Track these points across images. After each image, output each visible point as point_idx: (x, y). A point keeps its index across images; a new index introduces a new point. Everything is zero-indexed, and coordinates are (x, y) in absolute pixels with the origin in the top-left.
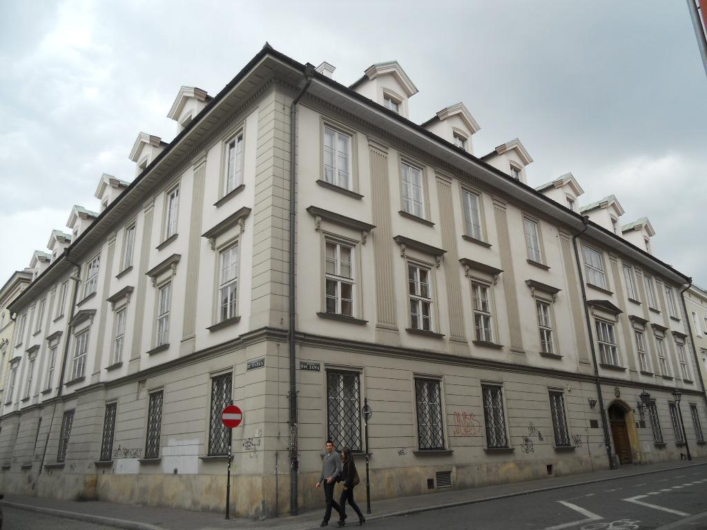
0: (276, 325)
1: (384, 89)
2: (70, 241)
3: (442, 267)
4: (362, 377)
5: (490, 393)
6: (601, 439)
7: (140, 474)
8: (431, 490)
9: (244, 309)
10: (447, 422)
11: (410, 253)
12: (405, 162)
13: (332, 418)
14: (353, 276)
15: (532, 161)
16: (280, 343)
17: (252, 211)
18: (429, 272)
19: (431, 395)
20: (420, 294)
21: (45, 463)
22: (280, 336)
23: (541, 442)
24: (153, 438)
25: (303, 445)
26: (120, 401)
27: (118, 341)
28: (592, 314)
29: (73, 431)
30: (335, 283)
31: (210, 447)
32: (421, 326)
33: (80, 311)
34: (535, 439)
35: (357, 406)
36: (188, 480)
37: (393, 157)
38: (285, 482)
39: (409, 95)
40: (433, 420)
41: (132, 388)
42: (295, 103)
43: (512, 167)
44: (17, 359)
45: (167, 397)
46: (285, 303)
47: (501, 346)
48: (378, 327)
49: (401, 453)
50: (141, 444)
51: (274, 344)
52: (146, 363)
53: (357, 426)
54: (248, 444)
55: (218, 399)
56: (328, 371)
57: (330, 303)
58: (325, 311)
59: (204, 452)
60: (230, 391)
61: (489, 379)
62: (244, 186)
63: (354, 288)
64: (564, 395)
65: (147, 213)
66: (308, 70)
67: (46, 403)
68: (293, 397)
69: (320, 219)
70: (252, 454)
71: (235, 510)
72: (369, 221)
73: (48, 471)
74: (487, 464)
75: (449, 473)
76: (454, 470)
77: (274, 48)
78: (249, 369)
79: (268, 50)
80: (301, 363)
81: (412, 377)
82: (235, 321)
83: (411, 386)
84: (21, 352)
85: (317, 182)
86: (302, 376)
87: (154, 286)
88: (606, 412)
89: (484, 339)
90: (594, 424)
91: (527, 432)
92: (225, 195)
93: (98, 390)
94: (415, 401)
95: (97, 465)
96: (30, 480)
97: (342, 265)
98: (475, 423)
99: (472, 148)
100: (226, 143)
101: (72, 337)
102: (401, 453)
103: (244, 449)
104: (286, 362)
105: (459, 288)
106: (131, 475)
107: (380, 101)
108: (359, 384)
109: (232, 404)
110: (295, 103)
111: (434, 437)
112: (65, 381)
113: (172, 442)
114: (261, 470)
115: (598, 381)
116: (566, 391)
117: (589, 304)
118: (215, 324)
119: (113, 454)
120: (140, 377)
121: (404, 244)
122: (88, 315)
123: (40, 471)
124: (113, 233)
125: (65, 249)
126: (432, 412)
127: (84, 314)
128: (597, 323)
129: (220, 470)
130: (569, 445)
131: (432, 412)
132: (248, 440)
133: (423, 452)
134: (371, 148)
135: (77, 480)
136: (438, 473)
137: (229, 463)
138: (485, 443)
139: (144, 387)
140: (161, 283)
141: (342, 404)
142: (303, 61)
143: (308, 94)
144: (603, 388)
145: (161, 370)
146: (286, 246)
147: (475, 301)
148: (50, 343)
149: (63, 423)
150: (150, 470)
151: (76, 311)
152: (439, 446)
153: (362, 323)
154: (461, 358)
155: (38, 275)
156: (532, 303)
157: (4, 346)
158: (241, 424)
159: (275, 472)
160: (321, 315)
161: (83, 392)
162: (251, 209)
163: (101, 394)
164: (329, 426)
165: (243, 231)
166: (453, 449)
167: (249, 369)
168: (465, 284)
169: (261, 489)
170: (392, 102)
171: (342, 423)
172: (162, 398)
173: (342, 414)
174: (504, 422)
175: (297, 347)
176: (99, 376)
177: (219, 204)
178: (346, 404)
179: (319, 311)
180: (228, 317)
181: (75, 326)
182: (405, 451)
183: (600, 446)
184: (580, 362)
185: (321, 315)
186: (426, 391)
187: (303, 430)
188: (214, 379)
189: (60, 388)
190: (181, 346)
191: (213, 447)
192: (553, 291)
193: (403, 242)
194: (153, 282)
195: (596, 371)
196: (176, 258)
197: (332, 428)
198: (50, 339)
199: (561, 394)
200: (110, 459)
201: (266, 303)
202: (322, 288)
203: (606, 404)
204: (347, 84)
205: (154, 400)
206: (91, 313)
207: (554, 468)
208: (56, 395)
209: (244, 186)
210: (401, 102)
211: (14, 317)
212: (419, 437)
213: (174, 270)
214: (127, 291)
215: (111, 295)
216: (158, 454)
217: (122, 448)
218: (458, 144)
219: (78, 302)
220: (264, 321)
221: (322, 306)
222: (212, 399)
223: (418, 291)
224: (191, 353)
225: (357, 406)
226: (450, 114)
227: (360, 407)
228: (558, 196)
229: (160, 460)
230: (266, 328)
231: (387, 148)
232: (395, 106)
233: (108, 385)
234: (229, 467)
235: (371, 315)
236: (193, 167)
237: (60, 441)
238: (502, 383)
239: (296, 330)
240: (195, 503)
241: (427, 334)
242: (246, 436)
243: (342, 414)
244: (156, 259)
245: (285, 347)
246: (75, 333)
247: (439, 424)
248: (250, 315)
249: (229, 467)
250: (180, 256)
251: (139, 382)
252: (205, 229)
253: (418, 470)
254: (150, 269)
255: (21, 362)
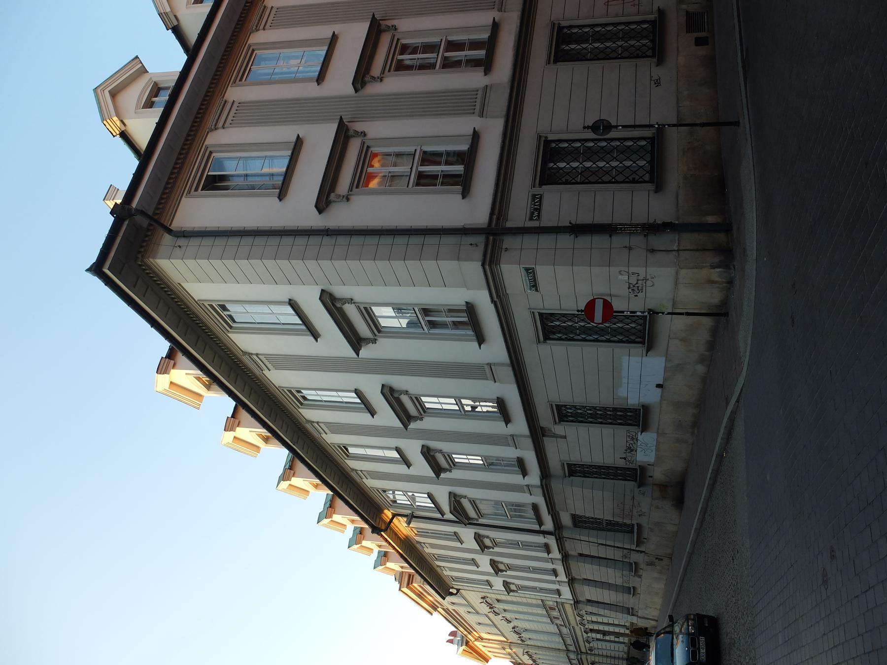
0: (479, 253)
2: (362, 528)
3: (395, 22)
4: (551, 137)
7: (657, 433)
9: (457, 297)
10: (617, 16)
11: (376, 70)
12: (242, 77)
14: (411, 149)
16: (504, 247)
17: (323, 288)
19: (580, 39)
20: (435, 55)
21: (634, 547)
22: (493, 247)
25: (640, 217)
26: (566, 458)
27: (492, 464)
29: (598, 515)
32: (481, 53)
33: (451, 512)
35: (591, 144)
36: (671, 370)
37: (235, 93)
40: (613, 37)
41: (549, 444)
42: (169, 231)
44: (506, 584)
45: (566, 398)
48: (481, 115)
49: (658, 83)
50: (621, 432)
51: (504, 256)
52: (519, 425)
53: (618, 143)
54: (634, 289)
56: (542, 184)
57: (449, 179)
59: (638, 349)
60: (564, 315)
62: (290, 300)
65: (327, 431)
66: (120, 213)
67: (561, 548)
68: (577, 230)
69: (332, 195)
70: (649, 283)
73: (643, 543)
75: (688, 14)
76: (684, 7)
77: (94, 261)
79: (96, 269)
80: (531, 219)
81: (553, 66)
82: (470, 309)
83: (565, 69)
84: (498, 582)
86: (547, 220)
87: (421, 419)
92: (304, 327)
93: (550, 487)
94: (587, 62)
96: (650, 564)
97: (395, 165)
100: (231, 327)
101: (482, 521)
102: (658, 83)
103: (641, 295)
104: (529, 241)
106: (658, 442)
108: (561, 141)
109: (582, 311)
110: (169, 231)
113: (622, 392)
114: (672, 270)
118: (475, 338)
119: (631, 466)
120: (537, 434)
121: (364, 77)
122: (456, 501)
123: (641, 552)
124: (353, 474)
125: (372, 532)
132: (630, 290)
133: (658, 54)
134: (227, 124)
135: (657, 508)
136: (688, 31)
137: (658, 313)
139: (550, 430)
141: (588, 164)
142: (109, 221)
143: (155, 214)
149: (586, 528)
150: (655, 417)
151: (452, 517)
153: (476, 137)
155: (406, 565)
157: (489, 600)
158: (609, 299)
159: (674, 253)
160: (465, 194)
161: (551, 503)
162: (323, 291)
163: (556, 485)
164: (617, 182)
165: (351, 301)
166: (655, 8)
167: (537, 290)
169: (695, 271)
170: (156, 96)
171: (614, 164)
173: (601, 164)
175: (509, 224)
177: (316, 336)
179: (461, 196)
181: (468, 518)
182: (655, 77)
185: (465, 194)
186: (573, 46)
187: (621, 217)
188: (547, 338)
189: (545, 533)
191: (633, 338)
193: (361, 78)
196: (386, 391)
197: (620, 178)
198: (483, 547)
200: (636, 469)
201: (448, 266)
202: (428, 193)
208: (553, 537)
209: (290, 300)
210: (156, 84)
211: (454, 591)
212: (638, 57)
213: (401, 394)
214: (428, 454)
215: (432, 474)
216: (636, 410)
217: (624, 456)
220: (474, 269)
221: (452, 192)
224: (510, 369)
225: (591, 144)
226: (168, 10)
229: (643, 406)
230: (483, 265)
232: (162, 92)
233: (545, 474)
234: (663, 313)
235: (464, 125)
239: (486, 226)
240: (701, 360)
242: (625, 292)
243: (601, 164)
246: (476, 517)
247: (620, 28)
249: (663, 313)
250: (383, 386)
251: (544, 435)
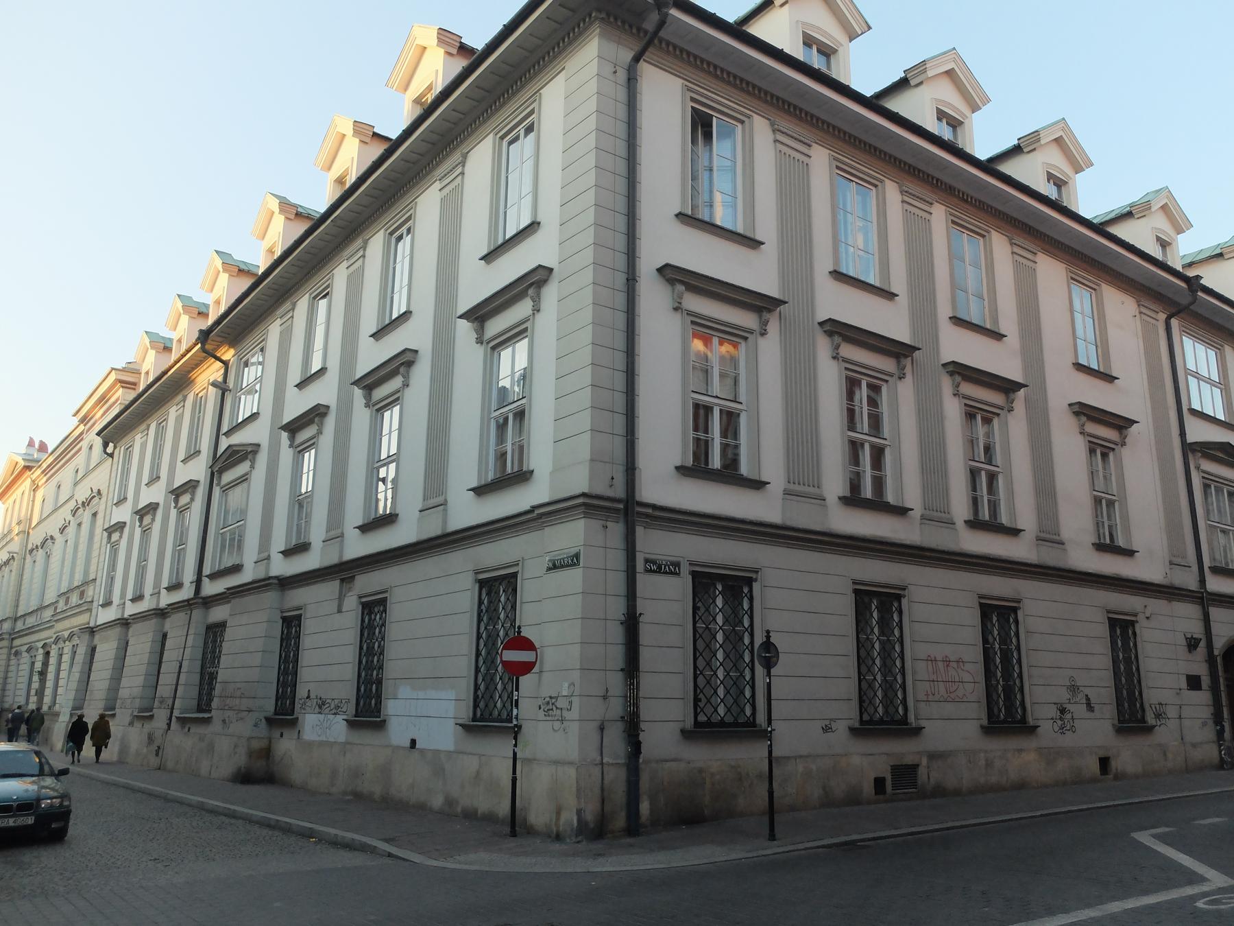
0: (601, 490)
1: (804, 23)
5: (995, 618)
6: (1206, 713)
8: (881, 797)
9: (540, 458)
10: (914, 673)
11: (849, 351)
13: (701, 663)
15: (1092, 165)
16: (609, 524)
18: (884, 389)
19: (884, 624)
21: (176, 713)
23: (1089, 715)
24: (368, 682)
25: (648, 710)
28: (1198, 468)
30: (708, 409)
31: (476, 706)
33: (229, 446)
34: (1079, 710)
35: (747, 641)
36: (437, 763)
38: (617, 778)
39: (852, 36)
40: (887, 669)
41: (329, 589)
42: (637, 59)
43: (1050, 177)
45: (396, 612)
46: (619, 445)
47: (1021, 530)
49: (826, 729)
50: (346, 691)
51: (596, 524)
52: (357, 546)
53: (748, 678)
54: (550, 706)
55: (490, 619)
56: (694, 574)
57: (701, 449)
58: (690, 462)
59: (465, 713)
60: (514, 607)
61: (996, 593)
62: (539, 223)
63: (743, 420)
64: (1137, 627)
67: (175, 607)
68: (631, 624)
70: (557, 725)
71: (525, 820)
72: (773, 292)
73: (183, 727)
74: (986, 751)
75: (914, 767)
76: (924, 761)
78: (549, 569)
80: (647, 561)
82: (523, 477)
85: (677, 215)
86: (646, 583)
87: (367, 405)
88: (1219, 660)
89: (985, 514)
90: (1194, 683)
91: (1063, 695)
95: (269, 721)
96: (151, 738)
98: (967, 678)
99: (972, 141)
100: (502, 138)
101: (217, 491)
102: (826, 729)
104: (617, 559)
105: (940, 419)
107: (794, 49)
108: (751, 599)
109: (519, 632)
111: (888, 701)
112: (207, 570)
113: (404, 691)
115: (1204, 600)
116: (1141, 618)
117: (1189, 449)
118: (483, 483)
119: (297, 706)
120: (344, 571)
122: (246, 453)
123: (169, 725)
125: (201, 331)
126: (886, 653)
127: (238, 452)
128: (1206, 487)
129: (497, 751)
130: (1143, 720)
131: (886, 653)
132: (548, 699)
137: (516, 738)
138: (984, 715)
139: (350, 589)
140: (382, 400)
141: (720, 637)
144: (1216, 613)
145: (377, 562)
146: (620, 343)
147: (972, 442)
148: (176, 501)
150: (367, 738)
152: (897, 717)
154: (943, 552)
155: (151, 379)
156: (1078, 446)
158: (536, 669)
160: (682, 470)
162: (551, 270)
163: (270, 598)
165: (537, 310)
166: (923, 723)
167: (549, 569)
168: (953, 410)
169: (574, 789)
170: (819, 51)
172: (385, 611)
173: (720, 655)
174: (1020, 676)
175: (640, 531)
176: (268, 565)
178: (726, 638)
179: (679, 464)
180: (509, 470)
181: (221, 471)
182: (834, 726)
183: (1204, 724)
184: (1171, 563)
185: (682, 470)
186: (875, 615)
187: (648, 683)
188: (482, 584)
189: (198, 583)
190: (419, 519)
191: (482, 704)
192: (1122, 424)
193: (838, 330)
194: (365, 397)
195: (1202, 581)
196: (408, 357)
198: (177, 493)
199: (1133, 623)
200: (292, 713)
201: (583, 449)
203: (1219, 644)
204: (731, 16)
205: (370, 614)
206: (249, 450)
207: (1115, 765)
212: (861, 701)
213: (404, 377)
214: (317, 414)
215: (287, 418)
216: (379, 711)
217: (312, 696)
218: (946, 133)
219: (225, 428)
220: (578, 482)
221: (684, 453)
222: (480, 620)
223: (864, 424)
224: (439, 532)
225: (747, 641)
227: (752, 643)
228: (1137, 234)
229: (384, 721)
230: (584, 495)
231: (810, 146)
232: (823, 59)
233: (286, 583)
234: (515, 745)
236: (438, 185)
237: (202, 674)
238: (1019, 601)
239: (638, 498)
240: (450, 802)
241: (879, 505)
243: (720, 655)
244: (371, 355)
245: (617, 529)
248: (551, 469)
249: (515, 745)
250: (416, 352)
251: (342, 580)
252: (464, 305)
253: (856, 760)
254: (358, 375)
255: (127, 530)
